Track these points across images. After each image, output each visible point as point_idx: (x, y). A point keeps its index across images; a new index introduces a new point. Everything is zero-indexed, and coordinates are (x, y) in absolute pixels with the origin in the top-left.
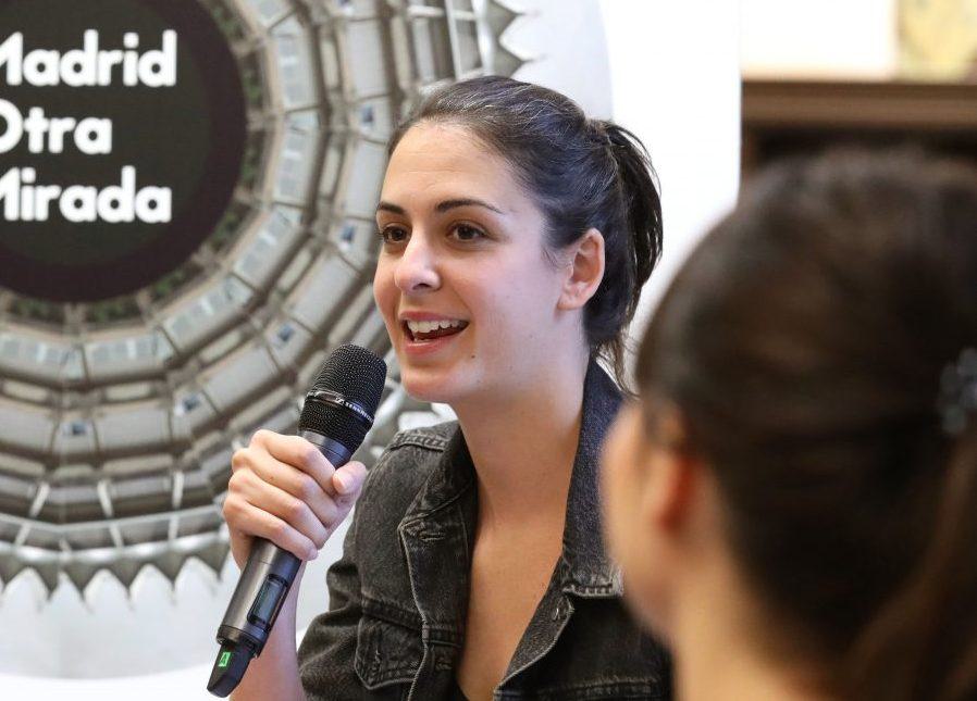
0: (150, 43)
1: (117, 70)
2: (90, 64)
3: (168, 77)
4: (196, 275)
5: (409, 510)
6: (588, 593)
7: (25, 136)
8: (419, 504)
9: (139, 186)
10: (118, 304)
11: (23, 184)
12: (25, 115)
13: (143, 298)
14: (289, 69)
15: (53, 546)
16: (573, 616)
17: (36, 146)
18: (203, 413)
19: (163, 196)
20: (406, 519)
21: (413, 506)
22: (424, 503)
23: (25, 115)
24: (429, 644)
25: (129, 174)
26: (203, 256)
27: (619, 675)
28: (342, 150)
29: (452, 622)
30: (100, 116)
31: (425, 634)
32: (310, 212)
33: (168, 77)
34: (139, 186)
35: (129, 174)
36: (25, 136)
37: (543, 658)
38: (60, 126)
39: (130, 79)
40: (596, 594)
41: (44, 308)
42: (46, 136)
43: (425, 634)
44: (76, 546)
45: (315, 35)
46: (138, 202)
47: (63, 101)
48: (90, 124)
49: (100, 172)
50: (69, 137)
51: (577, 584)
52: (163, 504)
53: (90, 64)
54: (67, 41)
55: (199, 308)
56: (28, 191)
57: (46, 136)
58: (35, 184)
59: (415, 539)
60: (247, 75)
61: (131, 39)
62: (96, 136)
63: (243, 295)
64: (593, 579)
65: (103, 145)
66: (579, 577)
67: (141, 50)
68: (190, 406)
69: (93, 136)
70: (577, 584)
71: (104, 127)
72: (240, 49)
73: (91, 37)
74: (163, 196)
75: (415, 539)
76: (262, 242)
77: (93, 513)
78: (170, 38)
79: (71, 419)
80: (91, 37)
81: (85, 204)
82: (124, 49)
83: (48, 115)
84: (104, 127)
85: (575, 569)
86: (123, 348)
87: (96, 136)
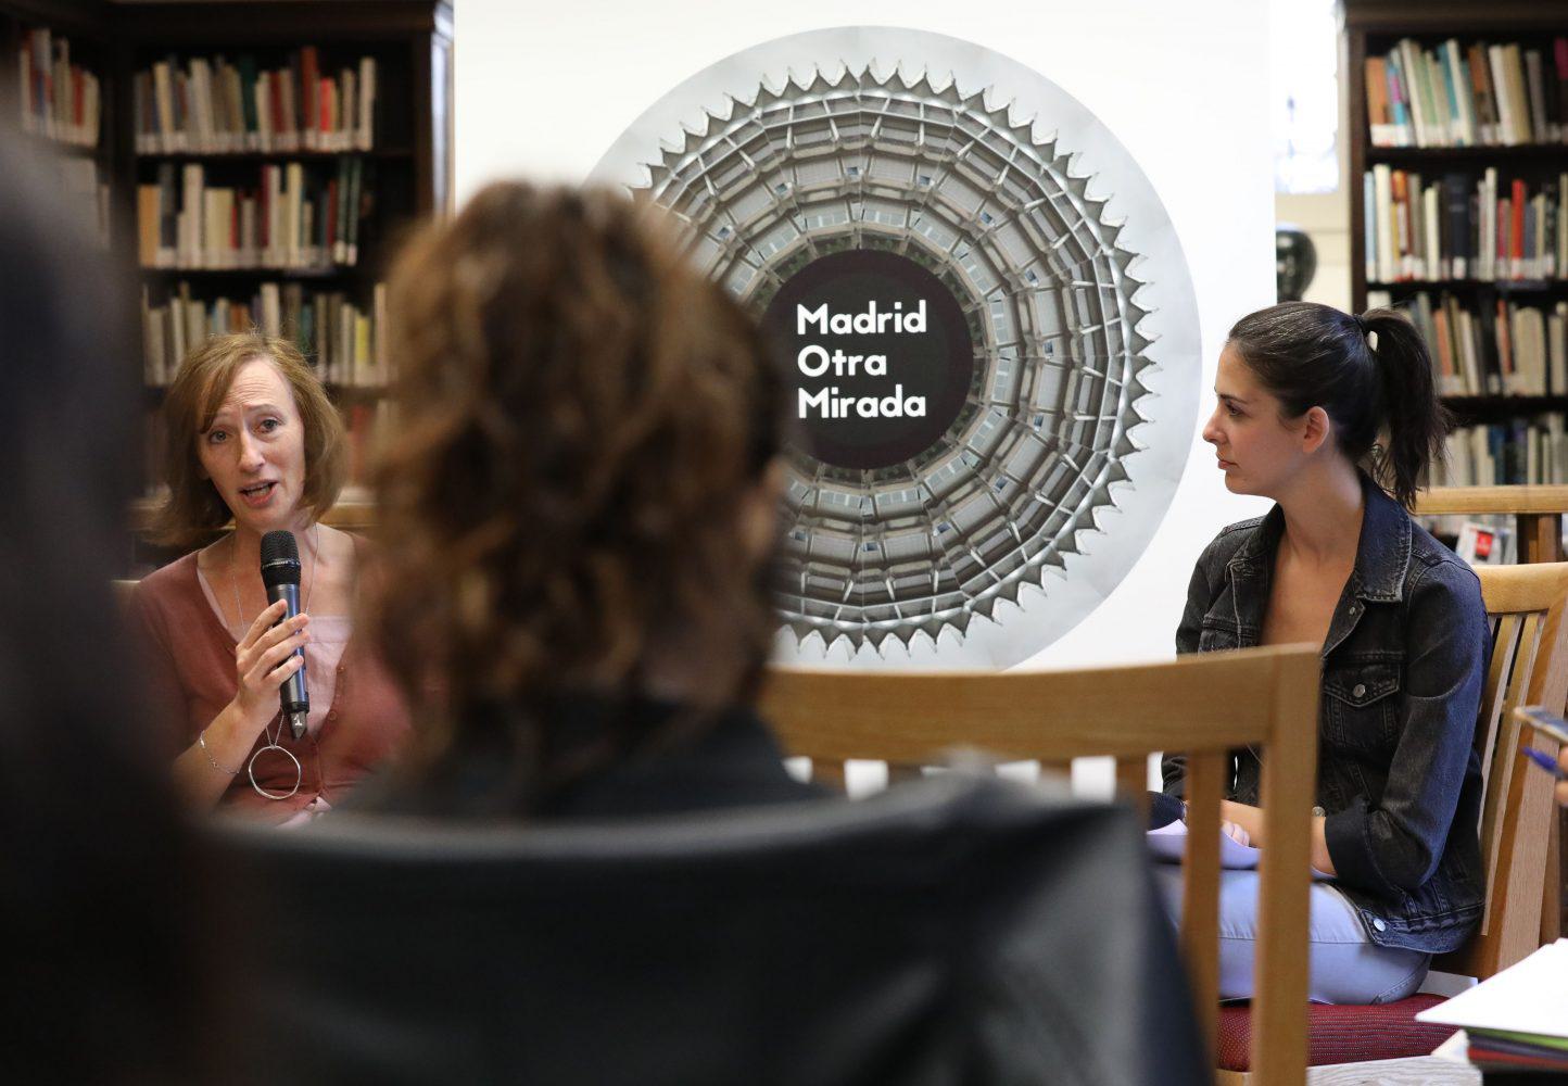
0: (911, 307)
1: (890, 324)
2: (873, 321)
3: (922, 327)
4: (943, 449)
5: (1236, 555)
6: (1375, 599)
7: (832, 366)
8: (1243, 553)
9: (905, 397)
10: (895, 469)
11: (831, 396)
12: (832, 354)
13: (910, 464)
14: (998, 320)
15: (858, 620)
16: (1365, 612)
17: (839, 372)
18: (951, 533)
19: (921, 401)
20: (1233, 560)
21: (1238, 554)
22: (1246, 553)
23: (832, 354)
24: (1242, 637)
25: (899, 388)
26: (948, 437)
27: (1384, 649)
28: (1034, 370)
29: (1256, 625)
30: (880, 354)
31: (1239, 631)
32: (1015, 408)
33: (922, 327)
34: (905, 397)
35: (899, 388)
36: (832, 366)
37: (1348, 638)
38: (853, 361)
39: (898, 329)
40: (1382, 599)
41: (848, 473)
42: (845, 366)
43: (1239, 631)
44: (872, 619)
45: (1014, 299)
46: (905, 405)
47: (855, 344)
48: (872, 359)
49: (881, 388)
50: (860, 366)
51: (1367, 594)
52: (927, 590)
53: (873, 321)
54: (858, 308)
55: (946, 470)
56: (835, 401)
57: (845, 366)
58: (839, 396)
59: (1239, 574)
60: (972, 325)
61: (898, 305)
62: (877, 365)
63: (973, 460)
64: (1378, 591)
65: (882, 370)
66: (1370, 590)
67: (904, 312)
68: (942, 531)
69: (875, 365)
70: (1367, 594)
71: (882, 360)
72: (967, 310)
73: (872, 305)
74: (921, 401)
75: (1239, 574)
76: (984, 429)
77: (883, 598)
78: (922, 304)
79: (866, 541)
80: (872, 305)
81: (871, 408)
82: (894, 311)
83: (846, 354)
84: (882, 360)
85: (1366, 585)
86: (898, 496)
87: (877, 365)
